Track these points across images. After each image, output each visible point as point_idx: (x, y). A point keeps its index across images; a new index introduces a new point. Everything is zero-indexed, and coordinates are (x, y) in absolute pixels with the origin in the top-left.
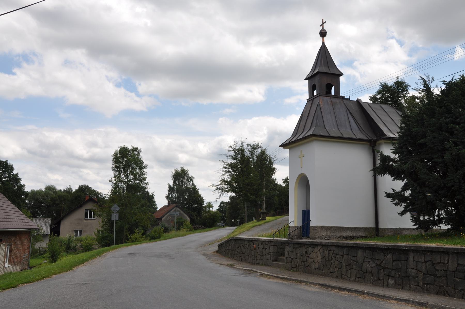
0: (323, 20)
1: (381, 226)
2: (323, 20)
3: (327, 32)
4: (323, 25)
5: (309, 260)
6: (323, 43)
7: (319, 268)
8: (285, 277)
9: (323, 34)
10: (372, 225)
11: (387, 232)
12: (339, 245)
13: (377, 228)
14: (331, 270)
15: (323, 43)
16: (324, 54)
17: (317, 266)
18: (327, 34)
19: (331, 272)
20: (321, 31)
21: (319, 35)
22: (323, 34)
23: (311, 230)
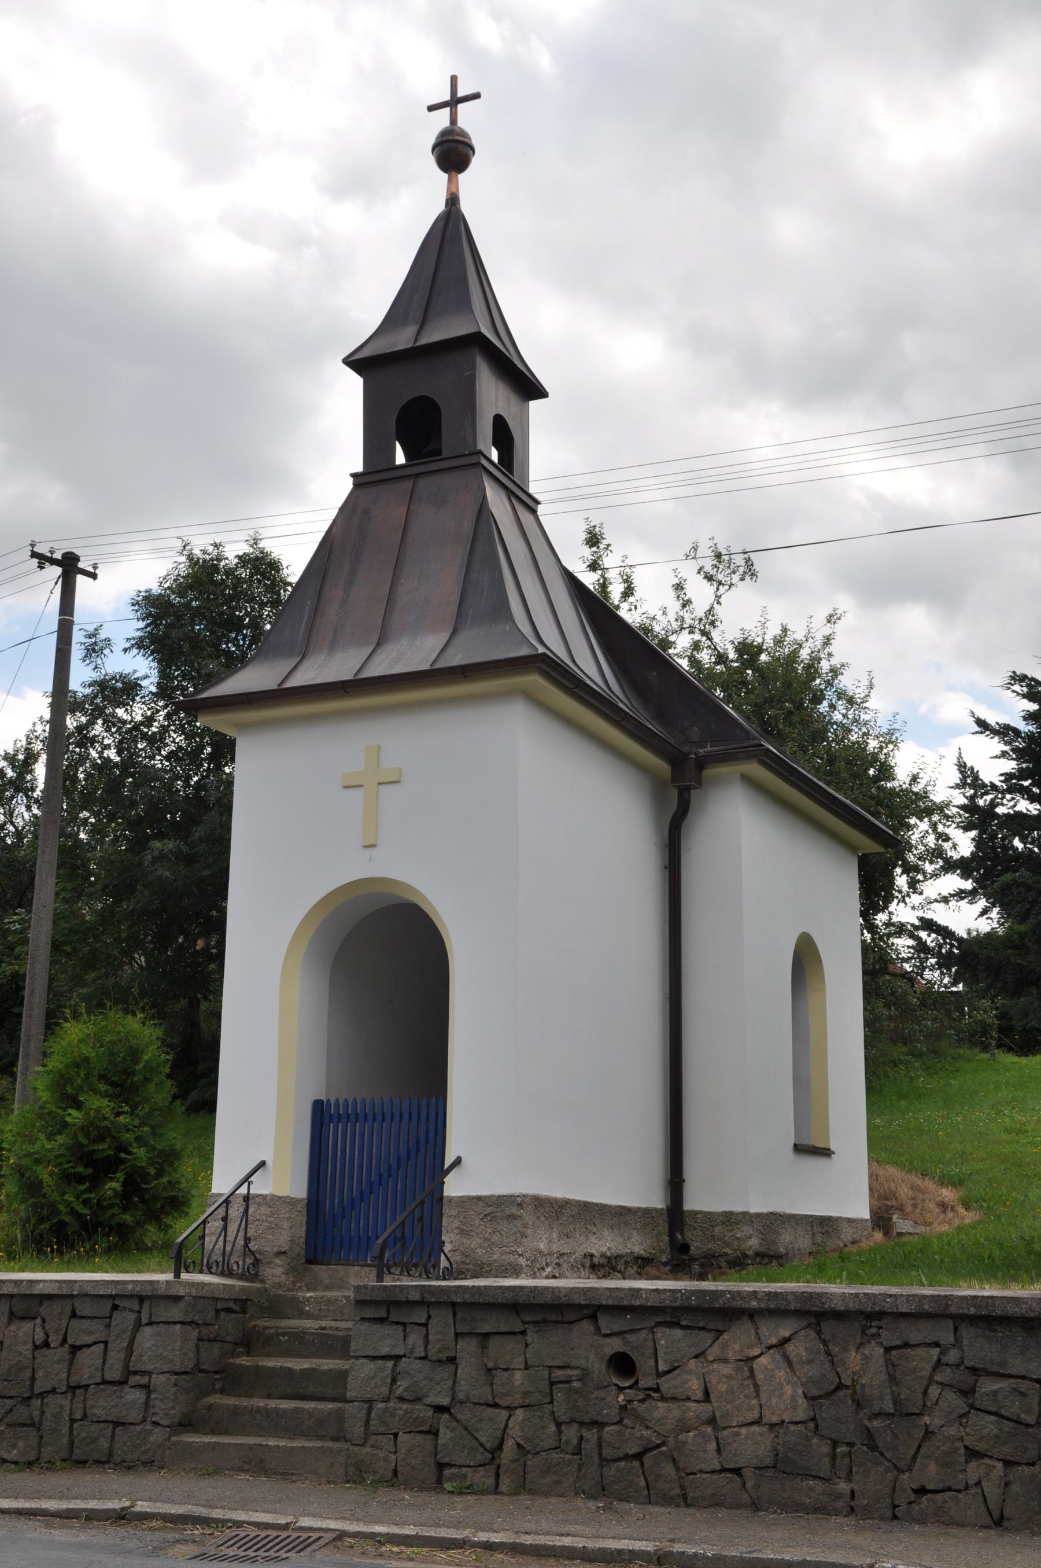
0: (454, 80)
1: (699, 1199)
2: (454, 80)
3: (475, 142)
4: (454, 102)
5: (660, 1409)
6: (453, 201)
7: (781, 1464)
8: (114, 1505)
9: (453, 153)
10: (646, 1193)
11: (744, 1231)
12: (1011, 1310)
13: (675, 1213)
14: (930, 1473)
15: (453, 201)
16: (448, 256)
17: (752, 1447)
18: (475, 161)
19: (921, 1491)
20: (444, 133)
21: (431, 161)
22: (453, 153)
23: (449, 1223)
